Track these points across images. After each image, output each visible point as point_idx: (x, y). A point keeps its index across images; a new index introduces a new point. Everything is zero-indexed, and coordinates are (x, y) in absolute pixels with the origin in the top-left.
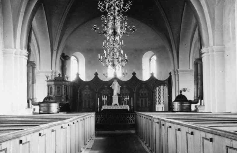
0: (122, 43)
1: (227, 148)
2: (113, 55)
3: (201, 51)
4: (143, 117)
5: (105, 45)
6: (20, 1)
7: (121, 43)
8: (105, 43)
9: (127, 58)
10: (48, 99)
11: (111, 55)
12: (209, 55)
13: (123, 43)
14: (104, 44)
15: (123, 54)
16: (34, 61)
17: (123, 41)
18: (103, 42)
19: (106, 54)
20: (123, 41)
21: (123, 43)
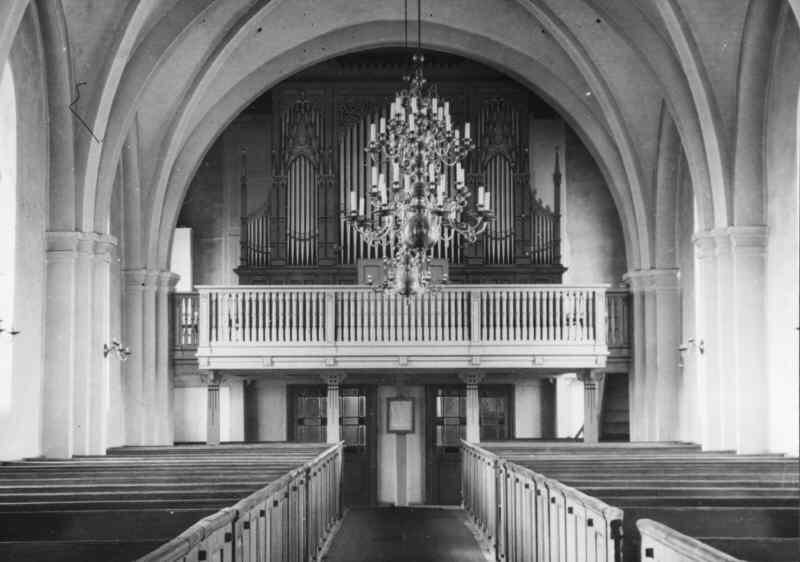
0: (462, 134)
1: (522, 239)
2: (419, 193)
3: (197, 355)
4: (484, 460)
5: (383, 143)
6: (126, 4)
7: (457, 133)
8: (383, 131)
9: (487, 208)
10: (759, 228)
11: (409, 189)
12: (729, 236)
13: (467, 135)
14: (373, 136)
15: (487, 208)
16: (566, 269)
17: (468, 126)
18: (373, 128)
19: (382, 188)
20: (468, 126)
21: (467, 135)
